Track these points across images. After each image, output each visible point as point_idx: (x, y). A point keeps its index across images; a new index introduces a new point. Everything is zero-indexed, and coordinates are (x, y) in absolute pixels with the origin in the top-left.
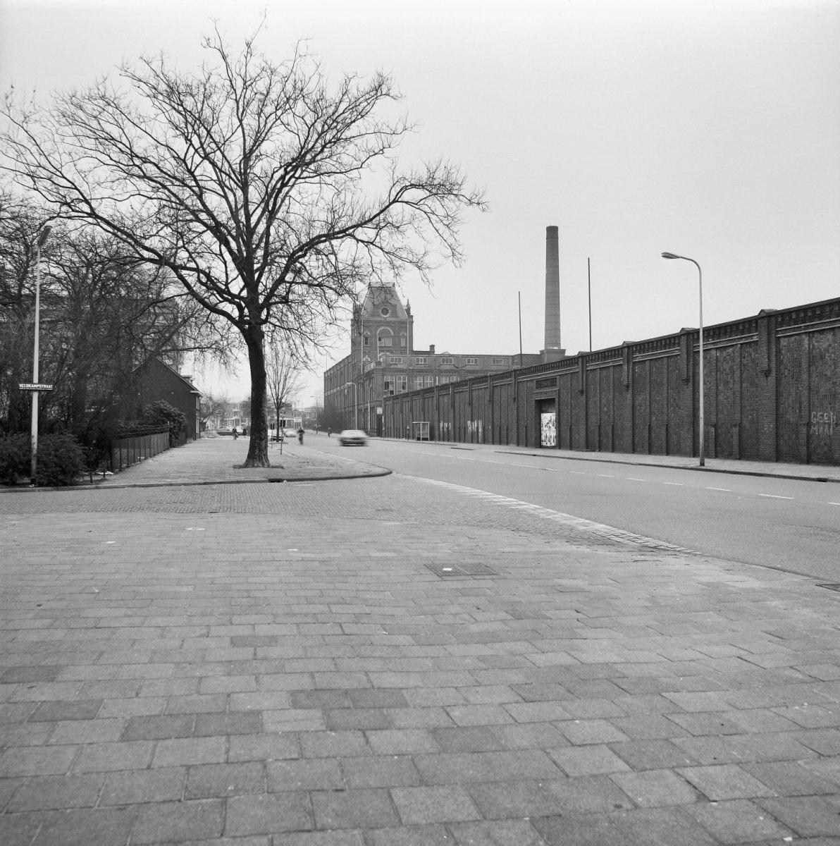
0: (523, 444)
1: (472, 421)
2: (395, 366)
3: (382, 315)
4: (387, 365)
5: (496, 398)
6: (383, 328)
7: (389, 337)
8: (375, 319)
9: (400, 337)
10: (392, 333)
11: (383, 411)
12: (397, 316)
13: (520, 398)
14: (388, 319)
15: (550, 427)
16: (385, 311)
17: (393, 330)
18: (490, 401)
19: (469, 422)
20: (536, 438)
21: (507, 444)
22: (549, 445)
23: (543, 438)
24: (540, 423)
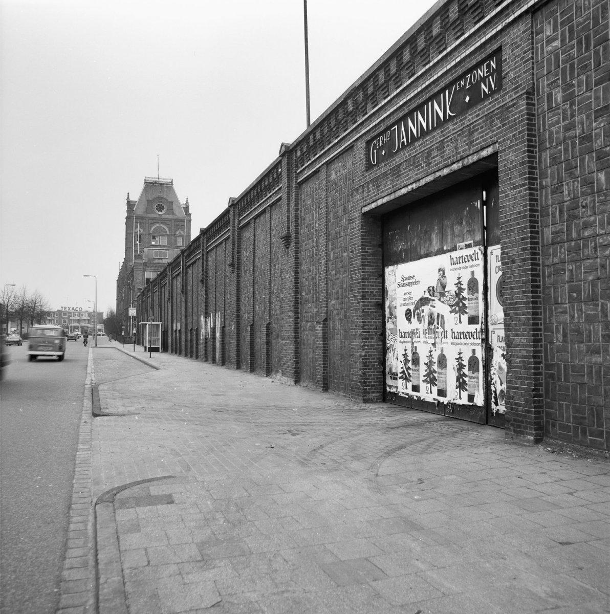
0: (313, 378)
1: (206, 316)
2: (160, 261)
3: (157, 212)
4: (149, 260)
5: (246, 255)
6: (158, 225)
7: (163, 235)
8: (149, 215)
9: (176, 236)
10: (168, 232)
11: (138, 312)
12: (173, 214)
13: (303, 231)
14: (163, 217)
15: (435, 321)
16: (160, 208)
17: (169, 231)
18: (232, 265)
19: (202, 318)
20: (365, 362)
21: (269, 371)
22: (428, 394)
23: (395, 363)
24: (381, 306)
